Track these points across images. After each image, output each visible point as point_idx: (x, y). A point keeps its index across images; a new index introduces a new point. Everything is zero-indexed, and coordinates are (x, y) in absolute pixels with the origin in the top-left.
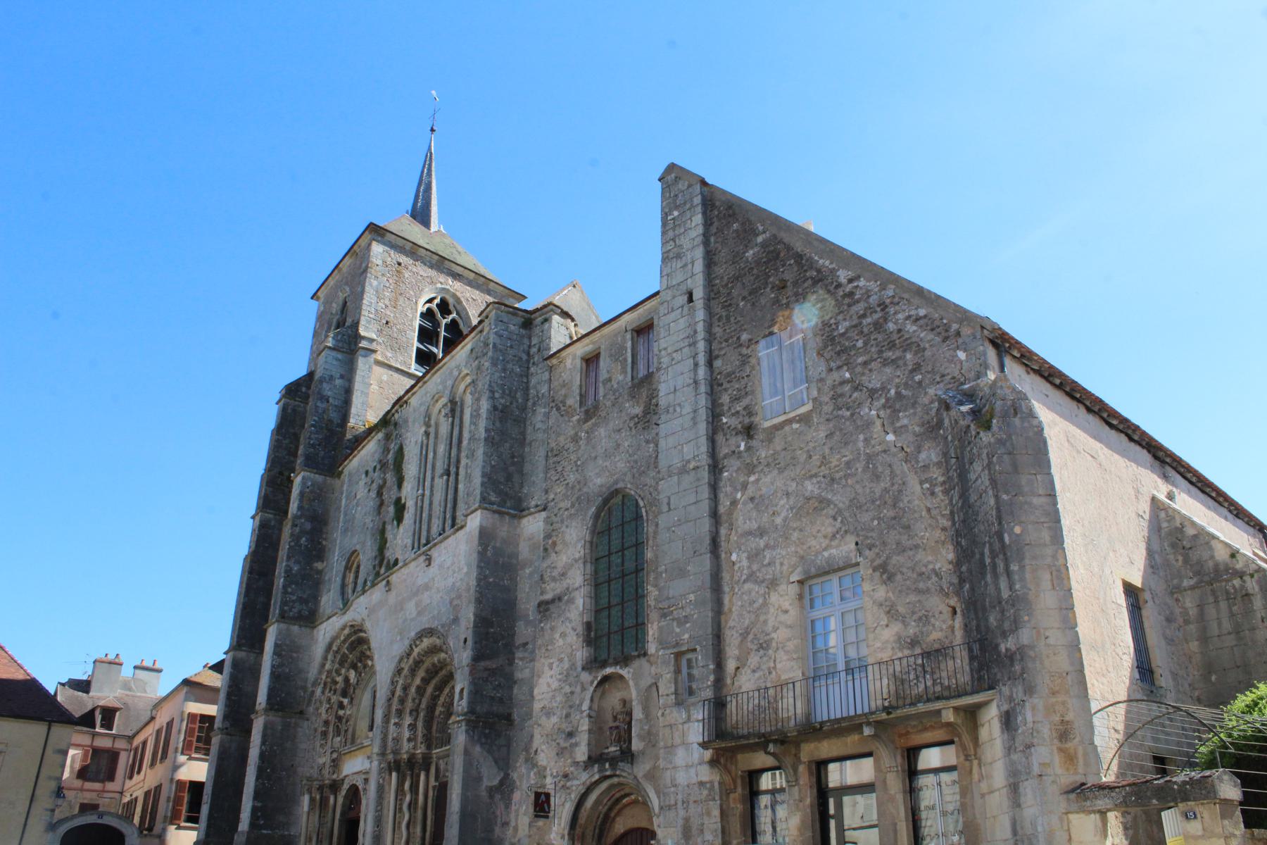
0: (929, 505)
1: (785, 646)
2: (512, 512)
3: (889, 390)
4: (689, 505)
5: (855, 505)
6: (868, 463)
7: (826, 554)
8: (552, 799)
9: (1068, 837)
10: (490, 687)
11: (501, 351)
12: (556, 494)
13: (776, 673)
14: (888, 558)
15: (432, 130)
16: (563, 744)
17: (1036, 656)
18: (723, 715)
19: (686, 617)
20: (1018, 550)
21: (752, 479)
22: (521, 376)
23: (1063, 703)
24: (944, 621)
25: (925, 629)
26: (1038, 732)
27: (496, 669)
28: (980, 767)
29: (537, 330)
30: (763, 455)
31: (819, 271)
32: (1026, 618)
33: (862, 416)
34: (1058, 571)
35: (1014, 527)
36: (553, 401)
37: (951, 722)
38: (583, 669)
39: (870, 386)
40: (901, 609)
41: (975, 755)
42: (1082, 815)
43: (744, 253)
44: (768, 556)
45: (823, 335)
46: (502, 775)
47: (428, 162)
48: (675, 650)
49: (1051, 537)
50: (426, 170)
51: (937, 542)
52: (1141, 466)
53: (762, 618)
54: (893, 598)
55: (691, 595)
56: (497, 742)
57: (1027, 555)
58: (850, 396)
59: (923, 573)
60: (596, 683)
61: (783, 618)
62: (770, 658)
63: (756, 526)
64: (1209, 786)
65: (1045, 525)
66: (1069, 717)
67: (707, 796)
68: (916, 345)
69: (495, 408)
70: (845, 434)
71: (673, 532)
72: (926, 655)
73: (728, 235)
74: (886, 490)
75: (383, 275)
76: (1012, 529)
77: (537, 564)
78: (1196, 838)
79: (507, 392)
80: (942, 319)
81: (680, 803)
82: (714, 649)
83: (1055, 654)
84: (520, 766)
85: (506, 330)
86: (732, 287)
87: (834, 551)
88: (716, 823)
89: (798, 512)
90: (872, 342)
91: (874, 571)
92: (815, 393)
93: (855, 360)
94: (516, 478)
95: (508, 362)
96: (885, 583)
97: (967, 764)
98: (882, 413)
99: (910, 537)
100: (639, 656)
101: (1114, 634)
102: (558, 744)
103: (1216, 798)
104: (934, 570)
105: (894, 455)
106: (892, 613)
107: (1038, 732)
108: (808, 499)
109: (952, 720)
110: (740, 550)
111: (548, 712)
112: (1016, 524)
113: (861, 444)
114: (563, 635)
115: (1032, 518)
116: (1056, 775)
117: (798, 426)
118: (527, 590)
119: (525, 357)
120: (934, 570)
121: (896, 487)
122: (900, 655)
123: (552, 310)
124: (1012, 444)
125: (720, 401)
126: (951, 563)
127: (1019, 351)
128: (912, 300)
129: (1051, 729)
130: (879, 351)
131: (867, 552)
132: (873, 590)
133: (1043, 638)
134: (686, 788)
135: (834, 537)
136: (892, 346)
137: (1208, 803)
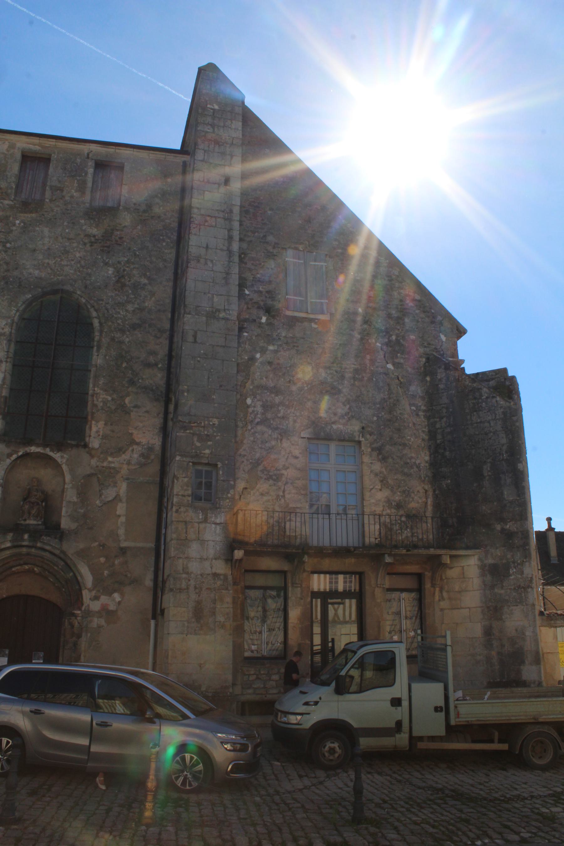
3: (391, 335)
4: (218, 346)
13: (285, 500)
19: (208, 435)
21: (271, 348)
24: (420, 498)
25: (407, 499)
30: (284, 334)
40: (390, 481)
42: (547, 628)
44: (282, 411)
54: (385, 473)
55: (215, 420)
59: (408, 463)
60: (15, 456)
62: (280, 488)
63: (272, 385)
71: (199, 361)
72: (408, 516)
96: (379, 460)
97: (432, 589)
100: (77, 446)
104: (415, 463)
106: (384, 482)
113: (367, 362)
120: (415, 463)
121: (392, 400)
126: (427, 462)
131: (368, 436)
132: (371, 463)
134: (199, 576)
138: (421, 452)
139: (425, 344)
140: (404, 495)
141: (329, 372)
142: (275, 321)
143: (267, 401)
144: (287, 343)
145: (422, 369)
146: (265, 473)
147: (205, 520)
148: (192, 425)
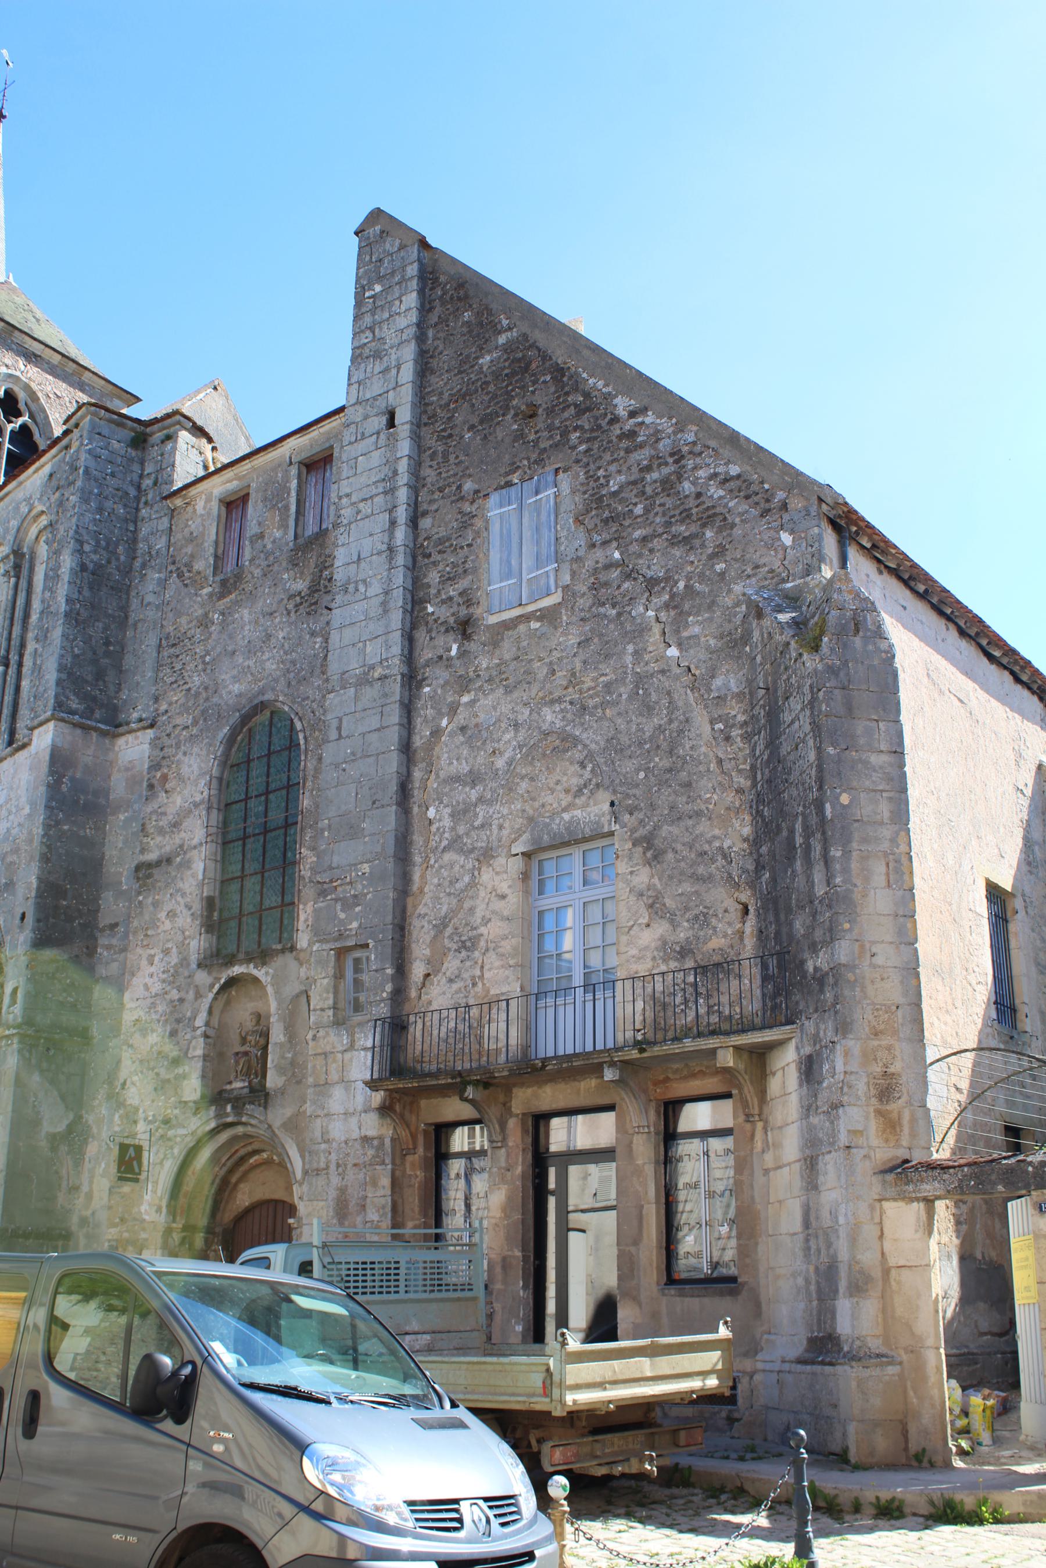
0: (720, 755)
2: (103, 726)
6: (637, 687)
7: (566, 816)
8: (145, 1154)
11: (96, 480)
12: (170, 704)
13: (484, 984)
17: (856, 980)
18: (402, 1043)
19: (355, 896)
20: (843, 827)
21: (465, 699)
22: (126, 520)
23: (889, 1048)
24: (729, 924)
25: (702, 933)
28: (766, 1133)
29: (154, 452)
30: (484, 666)
31: (587, 395)
32: (847, 926)
35: (840, 794)
38: (199, 966)
39: (650, 574)
40: (669, 902)
42: (901, 1204)
43: (477, 358)
46: (71, 1116)
48: (338, 945)
51: (728, 809)
52: (1028, 720)
53: (467, 905)
55: (366, 865)
57: (856, 836)
58: (619, 587)
60: (217, 987)
61: (498, 905)
62: (476, 963)
63: (467, 769)
65: (884, 794)
68: (721, 517)
69: (83, 568)
70: (607, 643)
71: (344, 770)
74: (660, 729)
76: (837, 798)
80: (762, 483)
81: (333, 1167)
82: (394, 946)
83: (882, 979)
85: (106, 448)
87: (578, 813)
89: (530, 753)
91: (634, 845)
92: (566, 579)
93: (630, 534)
94: (111, 677)
95: (106, 498)
97: (748, 1126)
98: (663, 616)
101: (967, 955)
102: (157, 1074)
104: (721, 848)
105: (677, 678)
106: (656, 907)
109: (731, 1064)
110: (441, 802)
112: (844, 791)
113: (629, 659)
114: (172, 915)
116: (870, 1147)
117: (538, 625)
118: (120, 845)
119: (133, 492)
120: (721, 848)
121: (675, 725)
122: (663, 968)
123: (179, 423)
124: (848, 674)
125: (425, 581)
126: (745, 840)
127: (870, 538)
128: (721, 451)
129: (868, 1084)
132: (632, 873)
133: (868, 955)
134: (343, 1145)
135: (579, 792)
136: (686, 516)
138: (734, 820)
139: (749, 571)
140: (696, 926)
141: (558, 709)
142: (472, 644)
143: (458, 803)
144: (490, 680)
145: (739, 630)
147: (351, 1047)
148: (335, 884)
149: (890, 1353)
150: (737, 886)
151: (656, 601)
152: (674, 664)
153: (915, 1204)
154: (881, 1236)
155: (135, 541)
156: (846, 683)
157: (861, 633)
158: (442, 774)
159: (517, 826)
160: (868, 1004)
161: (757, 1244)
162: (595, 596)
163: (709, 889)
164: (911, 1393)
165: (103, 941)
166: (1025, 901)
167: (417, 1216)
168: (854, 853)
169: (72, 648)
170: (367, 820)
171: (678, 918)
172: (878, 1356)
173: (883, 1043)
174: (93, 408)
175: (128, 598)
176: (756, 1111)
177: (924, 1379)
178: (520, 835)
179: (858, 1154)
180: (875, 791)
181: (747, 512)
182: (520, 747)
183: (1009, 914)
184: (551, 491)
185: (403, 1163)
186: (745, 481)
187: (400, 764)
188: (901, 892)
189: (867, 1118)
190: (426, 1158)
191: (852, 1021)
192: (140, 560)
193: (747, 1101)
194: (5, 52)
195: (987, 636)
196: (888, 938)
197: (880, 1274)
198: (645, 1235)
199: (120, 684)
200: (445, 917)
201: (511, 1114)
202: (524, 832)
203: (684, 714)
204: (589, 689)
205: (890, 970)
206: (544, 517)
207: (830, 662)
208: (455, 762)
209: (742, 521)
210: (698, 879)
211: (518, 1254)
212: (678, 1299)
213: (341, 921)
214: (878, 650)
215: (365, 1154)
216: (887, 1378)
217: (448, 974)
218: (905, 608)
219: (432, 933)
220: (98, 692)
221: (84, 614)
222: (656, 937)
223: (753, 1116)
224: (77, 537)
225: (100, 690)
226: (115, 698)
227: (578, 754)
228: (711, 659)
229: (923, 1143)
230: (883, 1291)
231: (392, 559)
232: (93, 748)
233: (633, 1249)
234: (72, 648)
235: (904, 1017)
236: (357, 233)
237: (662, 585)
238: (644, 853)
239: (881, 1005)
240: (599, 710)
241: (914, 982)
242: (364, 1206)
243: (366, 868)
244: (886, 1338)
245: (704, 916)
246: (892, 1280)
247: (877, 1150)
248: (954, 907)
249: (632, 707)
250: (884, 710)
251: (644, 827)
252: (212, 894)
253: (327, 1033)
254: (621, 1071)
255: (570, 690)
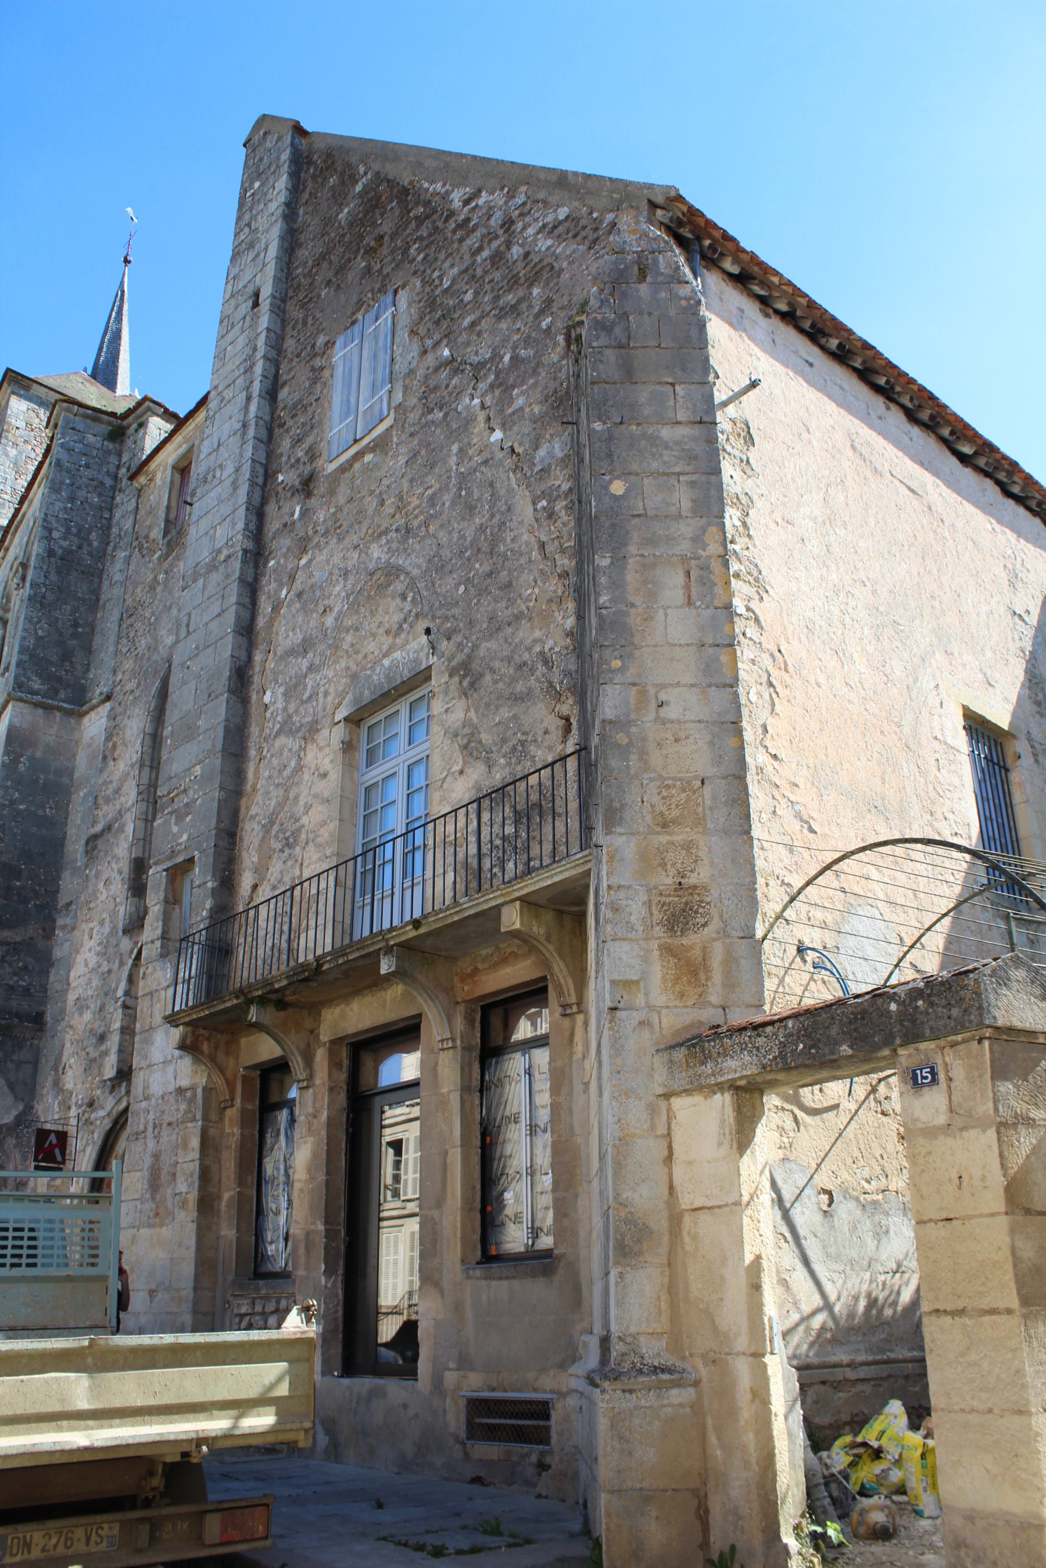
0: (543, 538)
1: (317, 836)
2: (65, 705)
5: (438, 566)
6: (460, 489)
7: (386, 662)
8: (72, 1141)
9: (666, 1153)
10: (8, 970)
11: (68, 471)
12: (123, 673)
14: (475, 647)
15: (127, 261)
16: (94, 1054)
17: (630, 744)
18: (226, 971)
19: (187, 805)
20: (613, 525)
22: (101, 508)
23: (688, 847)
24: (550, 748)
26: (616, 910)
27: (20, 943)
29: (129, 443)
30: (322, 519)
31: (427, 203)
32: (616, 664)
33: (459, 413)
34: (705, 568)
35: (611, 482)
36: (137, 539)
37: (518, 931)
38: (124, 932)
39: (476, 359)
40: (486, 738)
41: (578, 1004)
42: (697, 1099)
43: (337, 215)
45: (420, 301)
46: (21, 1107)
47: (117, 304)
48: (169, 864)
49: (693, 501)
50: (114, 314)
51: (550, 601)
52: (1027, 540)
53: (291, 795)
56: (15, 1057)
57: (635, 536)
58: (447, 386)
62: (296, 861)
63: (301, 637)
64: (967, 994)
65: (682, 478)
66: (701, 875)
67: (186, 1112)
68: (548, 269)
69: (51, 553)
70: (433, 450)
73: (321, 197)
74: (482, 529)
75: (26, 442)
76: (606, 487)
77: (92, 781)
78: (931, 1133)
79: (74, 530)
80: (591, 213)
81: (150, 1129)
82: (217, 854)
83: (677, 740)
84: (48, 1093)
85: (81, 442)
86: (316, 274)
87: (397, 655)
88: (193, 1161)
89: (357, 601)
90: (487, 287)
91: (451, 676)
92: (398, 397)
93: (460, 325)
94: (79, 657)
95: (79, 488)
97: (566, 1022)
98: (488, 400)
99: (511, 602)
101: (932, 794)
102: (88, 1053)
103: (981, 1025)
104: (542, 653)
105: (501, 463)
107: (616, 910)
108: (372, 574)
109: (517, 926)
110: (277, 683)
111: (81, 1005)
112: (618, 478)
114: (107, 882)
115: (655, 465)
116: (650, 1007)
118: (79, 822)
119: (108, 482)
120: (542, 653)
121: (495, 520)
123: (149, 409)
124: (628, 329)
125: (279, 451)
127: (736, 261)
128: (550, 199)
129: (649, 904)
130: (494, 297)
131: (444, 645)
132: (447, 711)
133: (653, 705)
134: (160, 1101)
136: (514, 282)
137: (964, 1041)
140: (513, 760)
146: (281, 836)
148: (172, 795)
149: (679, 1364)
150: (558, 696)
151: (483, 386)
152: (496, 449)
153: (718, 1096)
154: (669, 1159)
155: (109, 527)
156: (624, 341)
157: (648, 279)
158: (280, 651)
159: (341, 688)
160: (651, 780)
161: (576, 1196)
162: (424, 405)
163: (528, 707)
164: (713, 1439)
165: (60, 922)
166: (1032, 747)
167: (233, 1186)
168: (630, 561)
169: (36, 630)
170: (203, 716)
171: (494, 756)
172: (656, 1370)
173: (678, 838)
174: (65, 405)
175: (101, 582)
176: (573, 999)
177: (732, 1411)
178: (344, 698)
179: (628, 1019)
180: (668, 475)
181: (574, 251)
182: (348, 596)
183: (1009, 762)
184: (388, 314)
185: (221, 1119)
186: (573, 220)
187: (236, 647)
188: (710, 612)
189: (646, 960)
190: (243, 1112)
191: (623, 806)
192: (112, 544)
193: (560, 985)
194: (129, 210)
195: (948, 423)
196: (688, 678)
197: (665, 1224)
198: (449, 1191)
199: (89, 665)
200: (273, 814)
201: (320, 1044)
202: (347, 693)
203: (506, 503)
204: (414, 509)
205: (691, 725)
206: (381, 343)
207: (599, 317)
208: (291, 633)
209: (570, 263)
210: (516, 700)
211: (321, 1227)
212: (484, 1283)
213: (174, 835)
214: (675, 297)
215: (178, 1110)
216: (669, 1410)
217: (272, 880)
218: (811, 365)
219: (261, 834)
220: (63, 673)
221: (50, 597)
222: (470, 785)
223: (570, 1006)
224: (45, 524)
225: (66, 671)
226: (83, 678)
227: (399, 586)
228: (534, 429)
229: (748, 998)
230: (672, 1252)
231: (244, 434)
232: (56, 727)
233: (435, 1213)
234: (36, 630)
235: (714, 798)
236: (245, 145)
237: (488, 366)
238: (461, 682)
239: (675, 779)
240: (423, 529)
241: (733, 742)
242: (174, 1174)
243: (198, 770)
244: (676, 1339)
245: (522, 745)
246: (685, 1234)
247: (664, 1012)
248: (907, 730)
249: (454, 514)
250: (684, 370)
251: (462, 651)
252: (141, 855)
253: (155, 969)
254: (398, 959)
255: (398, 516)
